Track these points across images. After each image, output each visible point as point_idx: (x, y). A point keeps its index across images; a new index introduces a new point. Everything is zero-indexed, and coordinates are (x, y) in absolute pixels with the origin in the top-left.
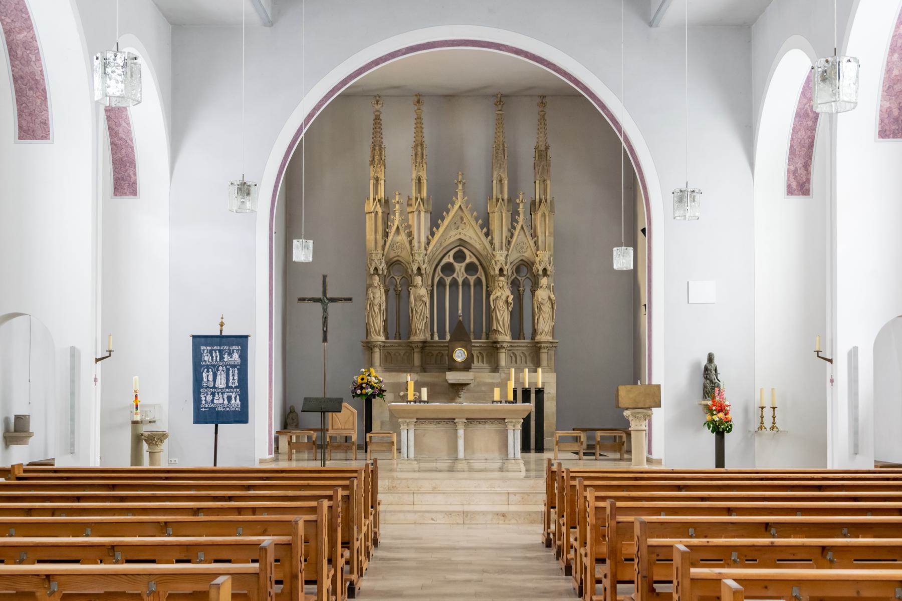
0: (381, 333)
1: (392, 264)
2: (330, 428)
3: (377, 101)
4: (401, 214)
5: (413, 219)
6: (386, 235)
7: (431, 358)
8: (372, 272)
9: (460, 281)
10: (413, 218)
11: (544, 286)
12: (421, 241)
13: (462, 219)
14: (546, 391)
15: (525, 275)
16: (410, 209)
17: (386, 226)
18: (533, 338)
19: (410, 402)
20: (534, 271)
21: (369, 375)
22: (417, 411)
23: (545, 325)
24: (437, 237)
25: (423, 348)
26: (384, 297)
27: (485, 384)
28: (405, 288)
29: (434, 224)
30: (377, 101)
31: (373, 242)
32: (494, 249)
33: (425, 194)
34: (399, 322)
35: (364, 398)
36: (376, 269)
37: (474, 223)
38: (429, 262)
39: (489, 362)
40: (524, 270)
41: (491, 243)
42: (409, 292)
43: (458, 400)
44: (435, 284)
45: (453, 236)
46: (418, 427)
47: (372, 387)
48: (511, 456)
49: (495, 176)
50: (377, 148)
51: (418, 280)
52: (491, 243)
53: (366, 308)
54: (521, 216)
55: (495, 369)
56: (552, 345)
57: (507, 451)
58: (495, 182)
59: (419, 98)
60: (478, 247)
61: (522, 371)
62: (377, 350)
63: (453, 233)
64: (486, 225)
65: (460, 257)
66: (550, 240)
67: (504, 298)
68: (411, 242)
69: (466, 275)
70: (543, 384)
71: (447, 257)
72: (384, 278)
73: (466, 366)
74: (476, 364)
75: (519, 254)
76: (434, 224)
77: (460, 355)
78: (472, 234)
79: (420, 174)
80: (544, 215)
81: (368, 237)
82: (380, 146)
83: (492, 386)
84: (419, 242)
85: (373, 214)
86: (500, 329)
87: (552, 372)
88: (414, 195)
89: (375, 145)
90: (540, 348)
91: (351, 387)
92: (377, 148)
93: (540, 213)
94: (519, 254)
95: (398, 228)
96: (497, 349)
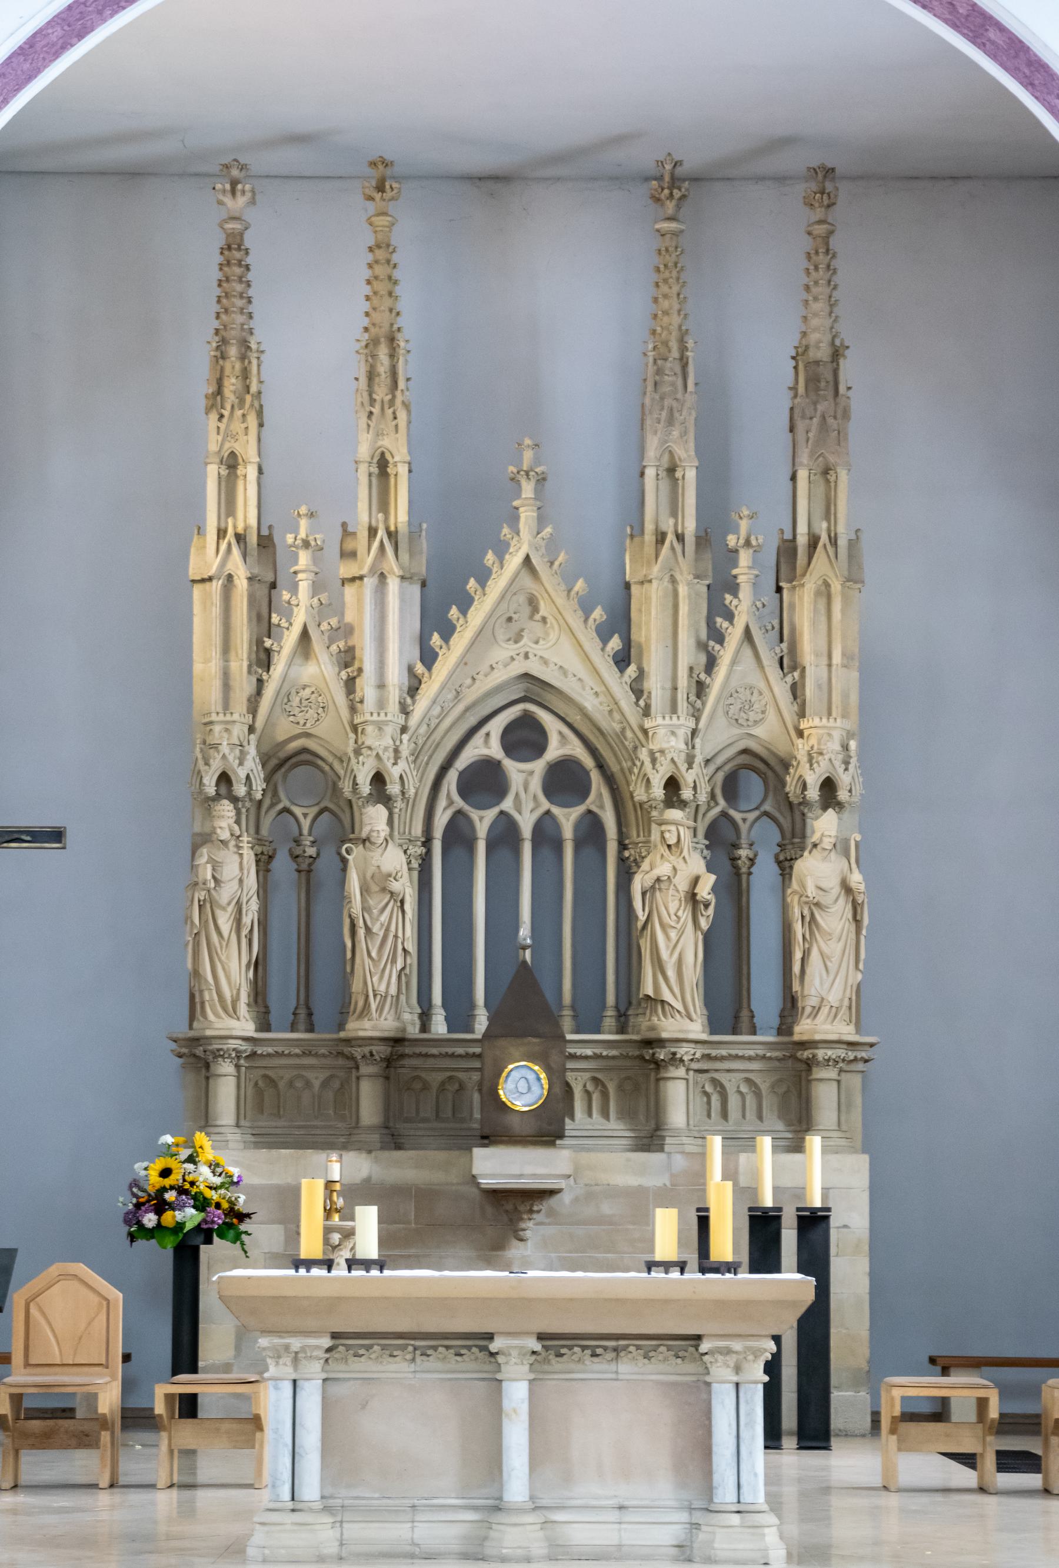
0: (243, 1009)
1: (285, 762)
2: (17, 1358)
3: (234, 183)
4: (316, 588)
5: (358, 605)
6: (264, 659)
7: (418, 1098)
8: (211, 790)
9: (526, 824)
10: (360, 600)
11: (827, 843)
12: (388, 691)
13: (533, 603)
14: (835, 1221)
15: (759, 805)
16: (347, 570)
17: (264, 626)
18: (785, 1028)
19: (309, 1264)
20: (791, 786)
21: (191, 1159)
22: (334, 1304)
23: (829, 982)
24: (443, 668)
25: (389, 1062)
26: (251, 881)
27: (615, 1193)
28: (328, 853)
29: (435, 622)
30: (234, 183)
31: (217, 684)
32: (647, 712)
33: (401, 515)
34: (305, 971)
35: (171, 1242)
36: (225, 779)
37: (575, 620)
38: (416, 755)
39: (627, 1114)
40: (753, 786)
41: (637, 690)
42: (344, 861)
43: (516, 1251)
44: (438, 833)
45: (503, 665)
46: (338, 1369)
47: (202, 1204)
48: (726, 1494)
49: (652, 451)
50: (233, 351)
51: (375, 819)
52: (637, 690)
53: (188, 918)
54: (745, 592)
55: (651, 1137)
56: (855, 1055)
57: (708, 1473)
58: (650, 472)
59: (383, 179)
60: (590, 703)
61: (750, 1145)
62: (226, 1068)
63: (502, 652)
64: (620, 625)
65: (525, 738)
66: (846, 681)
67: (682, 884)
68: (350, 685)
69: (546, 805)
70: (825, 1197)
71: (478, 739)
72: (253, 812)
73: (546, 1128)
74: (579, 1122)
75: (737, 731)
76: (435, 622)
77: (522, 1087)
78: (569, 657)
79: (386, 442)
80: (825, 592)
81: (198, 667)
82: (245, 345)
83: (640, 1205)
84: (381, 686)
85: (217, 586)
86: (667, 996)
87: (852, 1150)
88: (364, 518)
89: (224, 341)
90: (809, 1064)
91: (125, 1202)
92: (233, 351)
93: (810, 584)
94: (737, 731)
95: (305, 635)
96: (658, 1065)
